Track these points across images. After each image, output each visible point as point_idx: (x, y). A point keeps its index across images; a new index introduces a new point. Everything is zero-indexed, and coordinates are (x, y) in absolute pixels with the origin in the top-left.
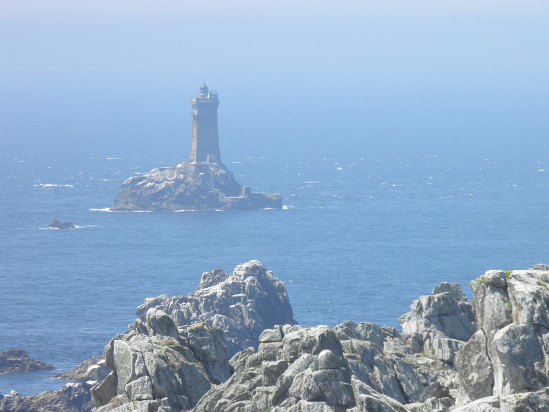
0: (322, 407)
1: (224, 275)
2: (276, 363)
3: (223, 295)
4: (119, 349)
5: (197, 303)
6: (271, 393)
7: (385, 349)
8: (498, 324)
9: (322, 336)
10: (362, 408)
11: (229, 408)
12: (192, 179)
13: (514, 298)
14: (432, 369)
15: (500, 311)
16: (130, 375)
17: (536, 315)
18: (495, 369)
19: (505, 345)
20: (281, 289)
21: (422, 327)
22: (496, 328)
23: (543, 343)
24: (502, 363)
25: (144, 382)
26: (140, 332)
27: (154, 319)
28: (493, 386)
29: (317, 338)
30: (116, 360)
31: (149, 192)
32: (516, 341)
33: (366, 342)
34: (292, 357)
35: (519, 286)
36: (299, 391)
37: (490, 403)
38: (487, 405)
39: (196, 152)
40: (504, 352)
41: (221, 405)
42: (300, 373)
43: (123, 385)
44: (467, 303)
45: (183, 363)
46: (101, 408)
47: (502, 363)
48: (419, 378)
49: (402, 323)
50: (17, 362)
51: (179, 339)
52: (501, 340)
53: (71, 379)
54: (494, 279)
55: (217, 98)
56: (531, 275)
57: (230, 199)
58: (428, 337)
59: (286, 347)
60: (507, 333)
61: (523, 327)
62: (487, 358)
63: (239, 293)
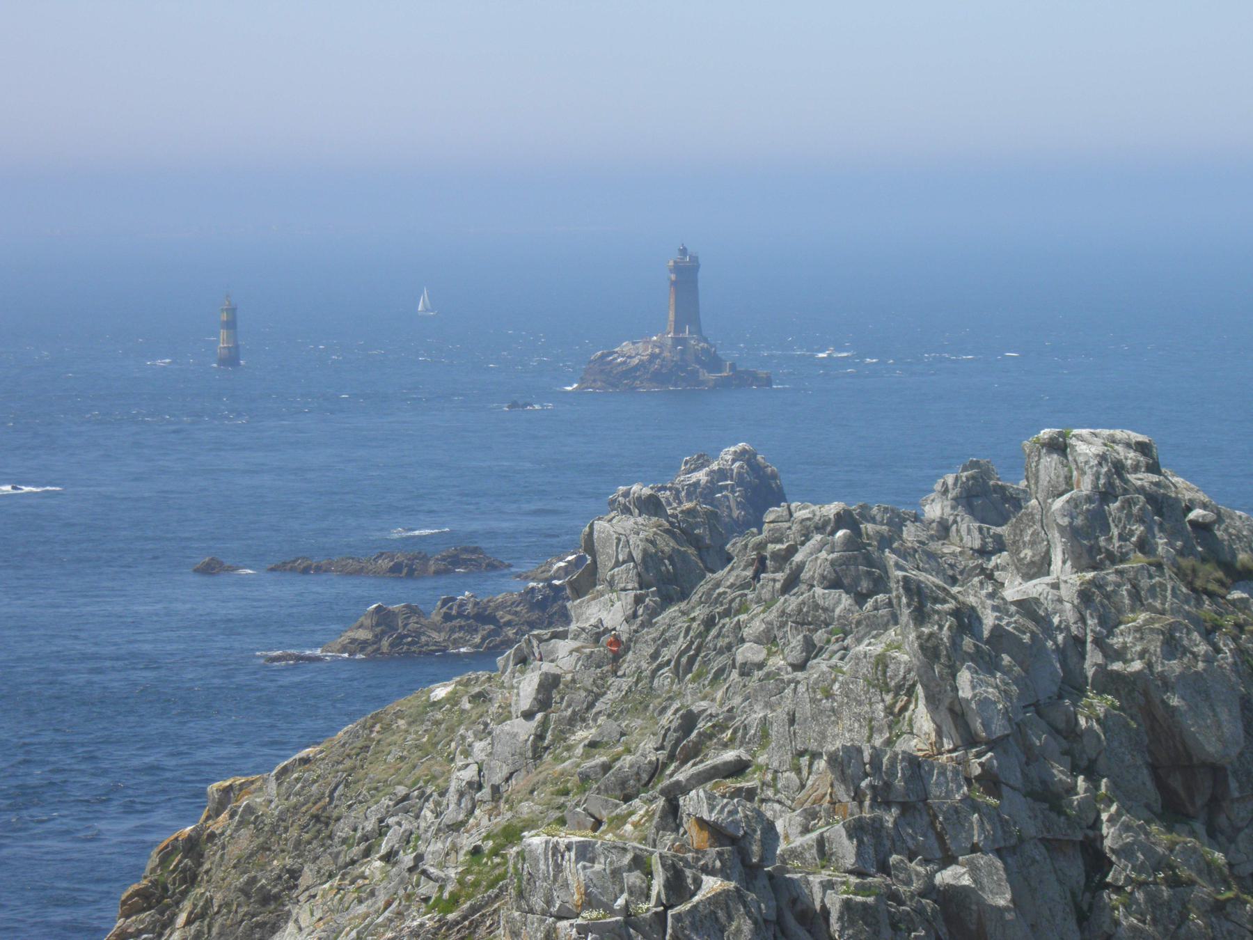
0: (840, 595)
1: (708, 461)
2: (784, 546)
3: (707, 482)
4: (600, 532)
5: (678, 492)
6: (778, 581)
7: (905, 535)
8: (1056, 492)
9: (838, 515)
10: (898, 587)
11: (729, 598)
12: (669, 354)
13: (1075, 461)
14: (960, 559)
15: (1058, 477)
16: (613, 561)
17: (1102, 481)
18: (1053, 545)
19: (1065, 516)
20: (774, 476)
21: (948, 510)
22: (1054, 497)
23: (1111, 514)
24: (1062, 537)
25: (630, 570)
26: (623, 513)
27: (639, 498)
28: (1049, 565)
29: (832, 516)
30: (596, 544)
31: (620, 369)
32: (1078, 511)
33: (883, 527)
34: (803, 538)
35: (1081, 448)
36: (813, 577)
37: (1048, 584)
38: (1044, 586)
39: (673, 323)
40: (1064, 525)
41: (720, 595)
42: (814, 557)
43: (605, 572)
44: (1000, 483)
45: (674, 548)
46: (579, 601)
47: (1062, 537)
48: (944, 569)
49: (925, 506)
50: (471, 560)
51: (668, 521)
52: (1060, 510)
53: (533, 580)
54: (1051, 439)
55: (698, 262)
56: (1095, 435)
57: (713, 376)
58: (955, 522)
59: (795, 527)
60: (1068, 502)
61: (1087, 495)
62: (1043, 532)
63: (727, 480)
